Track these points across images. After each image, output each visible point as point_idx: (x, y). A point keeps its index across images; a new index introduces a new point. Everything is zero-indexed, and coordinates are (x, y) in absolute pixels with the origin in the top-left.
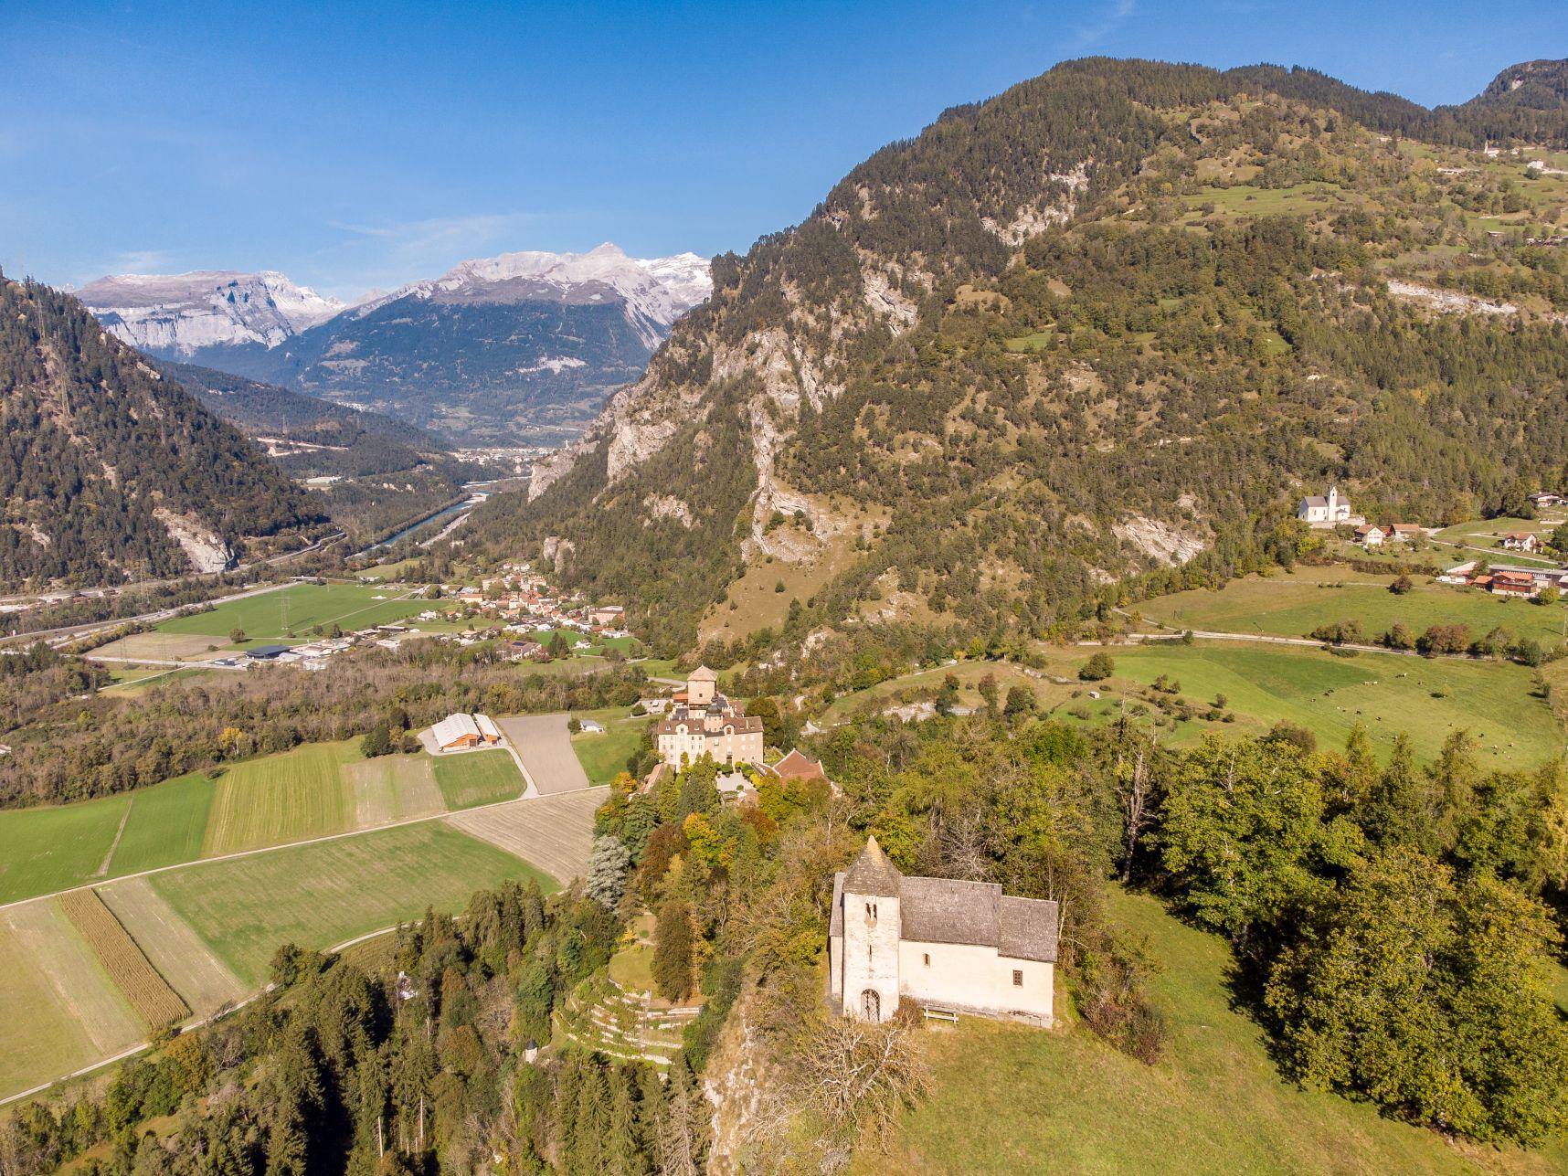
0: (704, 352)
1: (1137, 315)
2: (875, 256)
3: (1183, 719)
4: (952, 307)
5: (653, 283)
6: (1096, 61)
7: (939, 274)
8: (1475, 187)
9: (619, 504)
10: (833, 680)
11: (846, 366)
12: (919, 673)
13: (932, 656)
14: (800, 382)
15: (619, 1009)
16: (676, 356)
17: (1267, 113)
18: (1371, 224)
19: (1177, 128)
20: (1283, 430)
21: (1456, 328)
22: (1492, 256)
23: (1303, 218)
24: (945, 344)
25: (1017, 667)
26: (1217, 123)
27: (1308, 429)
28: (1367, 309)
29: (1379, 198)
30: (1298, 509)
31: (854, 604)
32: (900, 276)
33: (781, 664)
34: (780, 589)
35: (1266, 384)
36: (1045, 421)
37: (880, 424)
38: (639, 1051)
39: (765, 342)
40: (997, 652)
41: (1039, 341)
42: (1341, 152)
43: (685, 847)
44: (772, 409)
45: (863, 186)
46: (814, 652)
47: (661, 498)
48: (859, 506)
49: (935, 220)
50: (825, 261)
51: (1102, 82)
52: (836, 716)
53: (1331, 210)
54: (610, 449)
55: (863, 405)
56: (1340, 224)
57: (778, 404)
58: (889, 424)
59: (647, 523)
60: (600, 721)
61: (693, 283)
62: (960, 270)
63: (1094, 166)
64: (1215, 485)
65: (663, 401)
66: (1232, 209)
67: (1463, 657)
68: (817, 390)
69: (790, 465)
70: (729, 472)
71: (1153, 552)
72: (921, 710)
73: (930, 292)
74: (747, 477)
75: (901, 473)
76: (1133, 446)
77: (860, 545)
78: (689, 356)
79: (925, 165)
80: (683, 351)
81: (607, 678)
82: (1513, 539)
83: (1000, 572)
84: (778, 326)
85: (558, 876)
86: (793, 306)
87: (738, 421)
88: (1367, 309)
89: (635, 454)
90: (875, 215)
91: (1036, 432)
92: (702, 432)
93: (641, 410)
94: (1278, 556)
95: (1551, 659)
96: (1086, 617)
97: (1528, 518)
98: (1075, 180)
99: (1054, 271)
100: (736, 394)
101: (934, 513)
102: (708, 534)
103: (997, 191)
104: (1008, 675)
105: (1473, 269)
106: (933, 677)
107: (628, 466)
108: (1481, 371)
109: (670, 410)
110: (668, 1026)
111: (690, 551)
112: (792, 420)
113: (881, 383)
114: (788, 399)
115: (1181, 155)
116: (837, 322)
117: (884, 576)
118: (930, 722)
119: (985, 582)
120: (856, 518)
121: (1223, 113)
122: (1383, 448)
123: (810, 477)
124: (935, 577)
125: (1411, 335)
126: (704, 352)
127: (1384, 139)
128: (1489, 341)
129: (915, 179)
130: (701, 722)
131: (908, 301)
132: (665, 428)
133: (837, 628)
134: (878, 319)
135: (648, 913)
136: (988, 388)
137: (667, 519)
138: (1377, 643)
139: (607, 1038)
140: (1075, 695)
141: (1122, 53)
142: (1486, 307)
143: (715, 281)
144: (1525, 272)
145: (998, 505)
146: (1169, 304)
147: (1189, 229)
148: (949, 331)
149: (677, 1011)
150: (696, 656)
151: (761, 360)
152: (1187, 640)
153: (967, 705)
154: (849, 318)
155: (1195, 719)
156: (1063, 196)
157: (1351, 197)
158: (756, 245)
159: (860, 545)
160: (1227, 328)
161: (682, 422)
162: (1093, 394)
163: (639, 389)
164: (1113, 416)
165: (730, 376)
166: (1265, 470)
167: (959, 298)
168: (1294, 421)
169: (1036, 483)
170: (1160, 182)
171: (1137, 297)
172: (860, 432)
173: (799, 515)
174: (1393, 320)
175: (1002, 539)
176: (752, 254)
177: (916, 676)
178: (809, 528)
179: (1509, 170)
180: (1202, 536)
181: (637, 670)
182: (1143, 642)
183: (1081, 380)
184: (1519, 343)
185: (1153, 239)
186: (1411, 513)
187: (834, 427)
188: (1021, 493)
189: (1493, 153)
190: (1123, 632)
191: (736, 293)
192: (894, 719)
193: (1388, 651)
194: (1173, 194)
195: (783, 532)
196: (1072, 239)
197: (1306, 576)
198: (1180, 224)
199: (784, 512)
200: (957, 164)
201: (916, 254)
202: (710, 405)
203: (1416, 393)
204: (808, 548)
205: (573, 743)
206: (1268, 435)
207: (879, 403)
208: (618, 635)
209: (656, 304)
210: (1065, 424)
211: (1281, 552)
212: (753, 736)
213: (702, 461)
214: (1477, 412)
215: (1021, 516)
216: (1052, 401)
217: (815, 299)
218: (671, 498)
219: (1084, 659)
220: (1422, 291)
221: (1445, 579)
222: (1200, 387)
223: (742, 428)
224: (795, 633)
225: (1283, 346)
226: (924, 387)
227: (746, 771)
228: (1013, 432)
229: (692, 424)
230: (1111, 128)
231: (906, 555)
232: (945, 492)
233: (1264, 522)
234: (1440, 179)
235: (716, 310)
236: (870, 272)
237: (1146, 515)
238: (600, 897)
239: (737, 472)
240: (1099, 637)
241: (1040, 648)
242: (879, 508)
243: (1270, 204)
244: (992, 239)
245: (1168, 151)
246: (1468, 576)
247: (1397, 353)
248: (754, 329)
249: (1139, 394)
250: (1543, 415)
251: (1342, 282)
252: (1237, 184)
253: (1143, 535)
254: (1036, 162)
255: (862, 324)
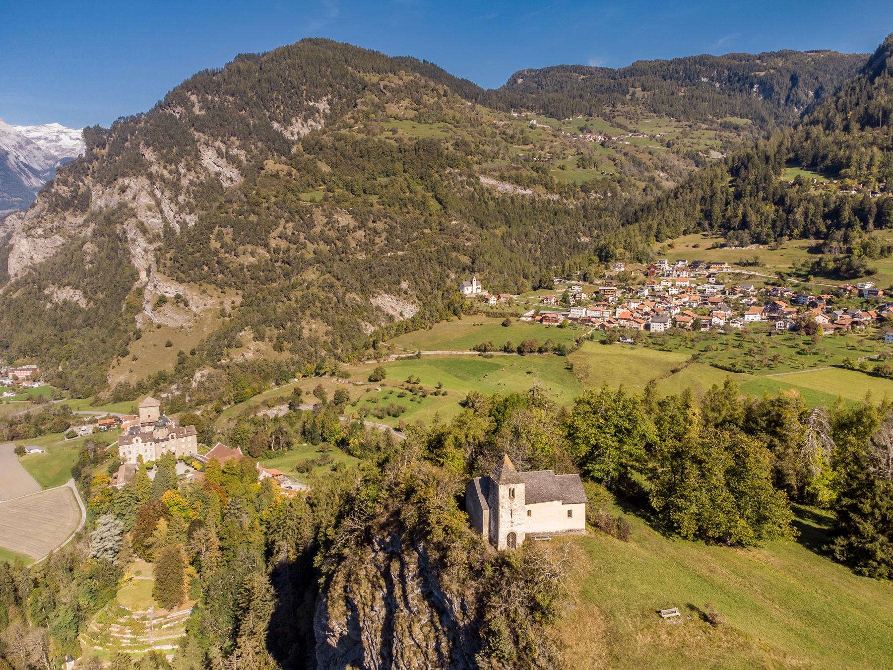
0: (83, 189)
1: (368, 185)
2: (206, 137)
3: (424, 396)
4: (263, 172)
5: (29, 142)
6: (325, 41)
7: (249, 151)
8: (510, 132)
9: (24, 293)
10: (220, 399)
11: (194, 203)
12: (276, 389)
13: (282, 378)
14: (162, 211)
15: (131, 624)
16: (61, 192)
17: (417, 83)
18: (469, 146)
19: (373, 85)
20: (444, 248)
21: (509, 200)
22: (520, 166)
23: (440, 141)
24: (263, 192)
25: (334, 379)
26: (393, 85)
27: (455, 248)
28: (472, 189)
29: (470, 133)
30: (460, 288)
31: (225, 351)
32: (224, 151)
33: (178, 393)
34: (169, 345)
35: (434, 225)
36: (328, 241)
37: (228, 239)
38: (150, 646)
39: (132, 184)
40: (322, 372)
41: (319, 196)
42: (451, 108)
43: (165, 512)
44: (143, 228)
45: (193, 94)
46: (201, 384)
47: (59, 288)
48: (220, 290)
49: (242, 120)
50: (172, 137)
51: (330, 53)
52: (225, 420)
53: (451, 138)
54: (11, 255)
55: (214, 227)
56: (456, 145)
57: (147, 225)
58: (234, 240)
59: (49, 306)
60: (40, 446)
61: (59, 144)
62: (262, 150)
63: (332, 100)
64: (417, 277)
65: (53, 222)
66: (409, 132)
67: (536, 354)
68: (175, 217)
69: (168, 265)
70: (113, 270)
71: (391, 312)
72: (280, 410)
73: (245, 162)
74: (128, 272)
75: (245, 270)
76: (375, 256)
77: (223, 314)
78: (71, 192)
79: (232, 86)
80: (65, 188)
81: (40, 415)
82: (547, 299)
83: (314, 326)
84: (142, 175)
85: (29, 553)
86: (151, 164)
87: (118, 236)
88: (472, 189)
89: (32, 258)
90: (203, 112)
91: (323, 247)
92: (89, 243)
93: (35, 227)
94: (454, 311)
95: (571, 352)
96: (367, 348)
97: (551, 289)
98: (322, 106)
99: (320, 156)
100: (113, 218)
101: (270, 293)
102: (102, 311)
103: (279, 107)
104: (330, 385)
105: (514, 172)
106: (286, 390)
107: (27, 266)
108: (521, 221)
109: (58, 228)
110: (169, 625)
111: (88, 323)
112: (158, 236)
113: (225, 215)
114: (155, 223)
115: (377, 100)
116: (185, 175)
117: (243, 332)
118: (287, 417)
119: (306, 333)
120: (219, 297)
121: (395, 81)
122: (487, 258)
123: (183, 272)
124: (276, 331)
125: (491, 203)
126: (83, 189)
127: (469, 104)
128: (523, 206)
129: (227, 93)
130: (151, 434)
131: (231, 166)
132: (56, 240)
133: (215, 367)
134: (212, 176)
135: (138, 560)
136: (293, 221)
137: (65, 302)
138: (501, 350)
139: (125, 642)
140: (368, 391)
141: (339, 38)
142: (520, 191)
143: (87, 143)
144: (535, 174)
145: (308, 288)
146: (383, 180)
147: (387, 141)
148: (264, 186)
149: (174, 614)
150: (108, 394)
151: (131, 196)
152: (418, 356)
153: (308, 405)
154: (193, 173)
155: (429, 396)
156: (317, 115)
157: (459, 132)
158: (116, 123)
159: (223, 314)
160: (412, 195)
161: (69, 236)
162: (351, 227)
163: (32, 213)
164: (363, 240)
165: (107, 206)
166: (439, 269)
167: (266, 167)
168: (448, 244)
169: (327, 276)
170: (369, 113)
171: (366, 175)
172: (215, 244)
173: (178, 297)
174: (481, 197)
175: (313, 308)
176: (114, 128)
177: (273, 390)
178: (186, 305)
179: (523, 124)
180: (414, 303)
181: (64, 408)
182: (398, 359)
183: (344, 219)
184: (534, 208)
185: (370, 144)
186: (505, 288)
187: (196, 241)
188: (320, 282)
189: (515, 115)
190: (387, 355)
191: (105, 152)
192: (266, 418)
193: (506, 354)
194: (376, 121)
195: (167, 308)
196: (327, 139)
197: (467, 320)
198: (382, 137)
199: (167, 295)
200: (252, 88)
201: (233, 139)
202: (92, 226)
203: (497, 231)
204: (187, 317)
205: (22, 463)
206: (438, 251)
207: (225, 227)
208: (36, 385)
209: (32, 156)
210: (338, 243)
211: (456, 309)
212: (189, 438)
213: (91, 262)
214: (522, 240)
215: (322, 295)
216: (329, 230)
217: (167, 160)
218: (68, 288)
219: (370, 371)
220: (494, 182)
221: (523, 319)
222: (404, 225)
223: (121, 240)
224: (186, 372)
225: (439, 207)
226: (253, 218)
227: (187, 461)
228: (311, 247)
229: (79, 238)
230: (338, 80)
231: (256, 319)
232: (275, 281)
233: (446, 295)
234: (495, 126)
235: (90, 162)
236: (204, 146)
237: (386, 293)
238: (104, 556)
239: (120, 269)
240: (376, 358)
241: (345, 367)
242: (233, 291)
243: (424, 132)
244: (280, 135)
245: (370, 97)
246: (533, 317)
247: (486, 211)
248: (123, 176)
249: (374, 228)
250: (547, 242)
251: (460, 175)
252: (407, 119)
253: (385, 303)
254: (299, 93)
255: (202, 177)
